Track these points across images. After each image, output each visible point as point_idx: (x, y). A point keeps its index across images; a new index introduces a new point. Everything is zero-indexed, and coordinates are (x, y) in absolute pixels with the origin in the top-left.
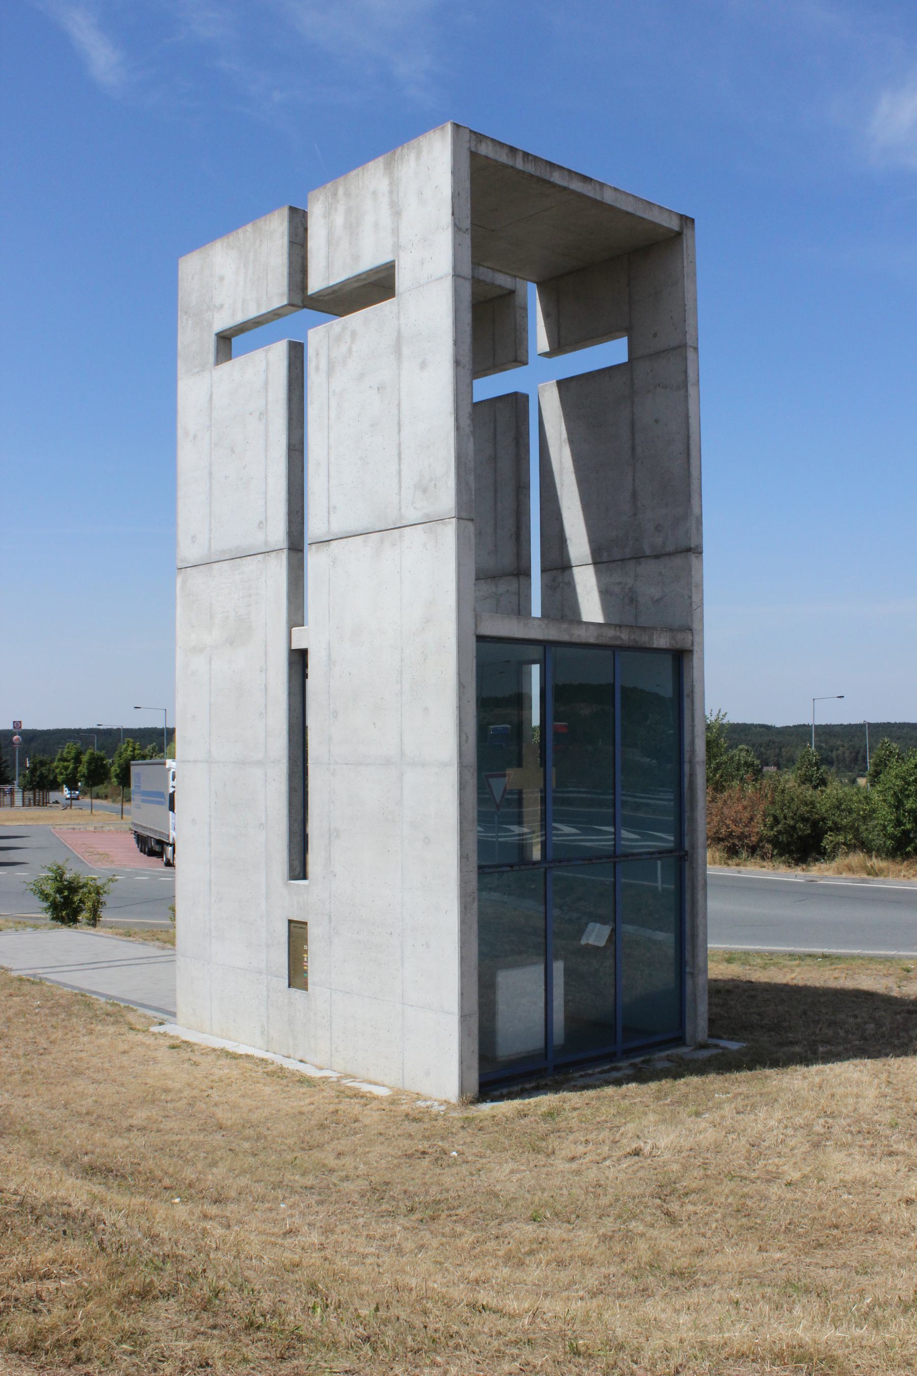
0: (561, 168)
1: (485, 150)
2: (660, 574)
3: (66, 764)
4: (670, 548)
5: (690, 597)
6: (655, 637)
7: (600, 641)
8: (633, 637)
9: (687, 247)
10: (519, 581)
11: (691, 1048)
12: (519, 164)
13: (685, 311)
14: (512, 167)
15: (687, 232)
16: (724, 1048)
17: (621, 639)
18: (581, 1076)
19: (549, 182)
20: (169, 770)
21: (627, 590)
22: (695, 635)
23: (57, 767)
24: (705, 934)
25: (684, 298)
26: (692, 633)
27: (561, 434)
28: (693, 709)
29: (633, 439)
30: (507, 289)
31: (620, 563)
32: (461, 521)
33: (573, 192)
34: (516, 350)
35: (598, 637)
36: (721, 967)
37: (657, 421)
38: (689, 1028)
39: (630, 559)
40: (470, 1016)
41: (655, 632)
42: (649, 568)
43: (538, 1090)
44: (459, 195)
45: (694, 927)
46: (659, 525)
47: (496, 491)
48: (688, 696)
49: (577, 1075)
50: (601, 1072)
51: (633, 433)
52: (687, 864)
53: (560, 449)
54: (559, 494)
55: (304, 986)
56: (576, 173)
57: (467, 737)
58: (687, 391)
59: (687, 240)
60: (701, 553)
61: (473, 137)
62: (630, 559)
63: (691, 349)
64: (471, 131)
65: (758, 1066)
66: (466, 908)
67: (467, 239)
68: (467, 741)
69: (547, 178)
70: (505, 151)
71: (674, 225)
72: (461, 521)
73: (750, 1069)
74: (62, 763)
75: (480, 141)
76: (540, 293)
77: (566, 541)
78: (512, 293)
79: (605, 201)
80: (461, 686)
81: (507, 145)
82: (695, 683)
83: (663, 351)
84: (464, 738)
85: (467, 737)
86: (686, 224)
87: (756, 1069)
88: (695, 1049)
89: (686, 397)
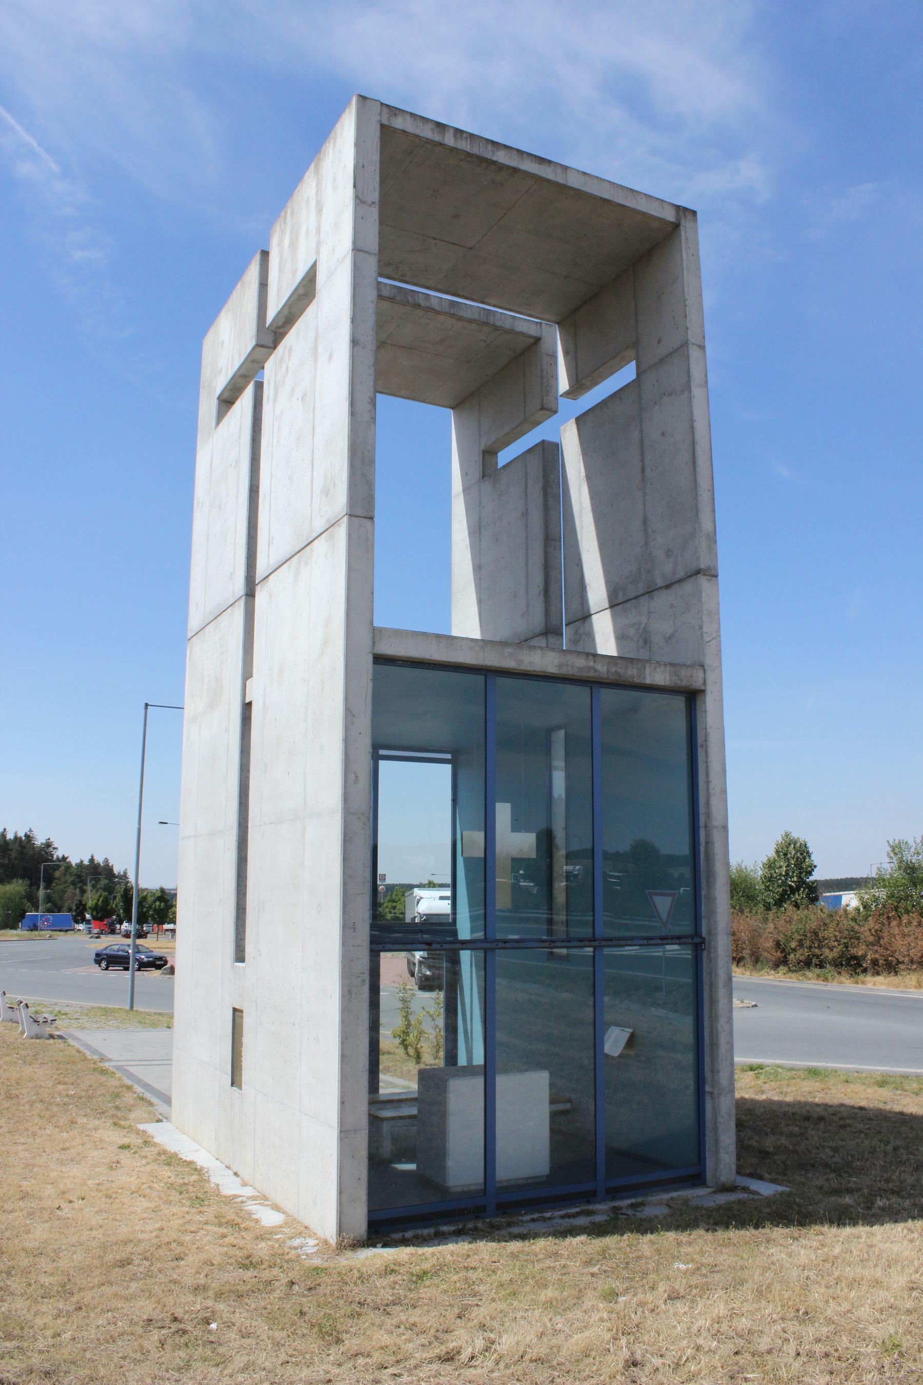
0: (506, 147)
1: (399, 123)
2: (672, 606)
3: (394, 904)
4: (680, 574)
5: (701, 627)
6: (647, 672)
7: (564, 671)
8: (613, 670)
9: (687, 239)
10: (547, 640)
11: (710, 1190)
12: (449, 140)
13: (686, 306)
14: (441, 144)
15: (686, 224)
16: (755, 1193)
17: (596, 671)
18: (533, 1220)
19: (494, 163)
20: (416, 897)
21: (641, 631)
22: (707, 673)
23: (387, 907)
24: (730, 1043)
25: (684, 292)
26: (704, 670)
27: (580, 473)
28: (707, 762)
29: (643, 461)
30: (530, 337)
31: (634, 601)
32: (354, 519)
33: (527, 174)
34: (543, 397)
35: (560, 666)
36: (869, 1091)
37: (663, 434)
38: (709, 1164)
39: (644, 594)
40: (355, 1131)
41: (647, 665)
42: (662, 600)
43: (440, 1238)
44: (363, 166)
45: (714, 1034)
46: (669, 550)
47: (527, 549)
48: (702, 746)
49: (527, 1218)
50: (562, 1217)
51: (642, 454)
52: (705, 953)
53: (580, 489)
54: (579, 537)
55: (240, 1088)
56: (529, 154)
57: (357, 777)
58: (690, 392)
59: (686, 232)
60: (716, 576)
61: (385, 110)
62: (644, 594)
63: (695, 347)
64: (382, 104)
65: (768, 1223)
66: (350, 992)
67: (374, 214)
68: (356, 782)
69: (489, 156)
70: (429, 126)
71: (670, 216)
72: (356, 520)
73: (756, 1227)
74: (390, 904)
75: (395, 115)
76: (560, 333)
77: (586, 587)
78: (537, 340)
79: (570, 184)
80: (349, 714)
81: (432, 121)
82: (708, 730)
83: (667, 357)
84: (352, 777)
85: (357, 777)
86: (685, 215)
87: (764, 1227)
88: (714, 1192)
89: (690, 398)
